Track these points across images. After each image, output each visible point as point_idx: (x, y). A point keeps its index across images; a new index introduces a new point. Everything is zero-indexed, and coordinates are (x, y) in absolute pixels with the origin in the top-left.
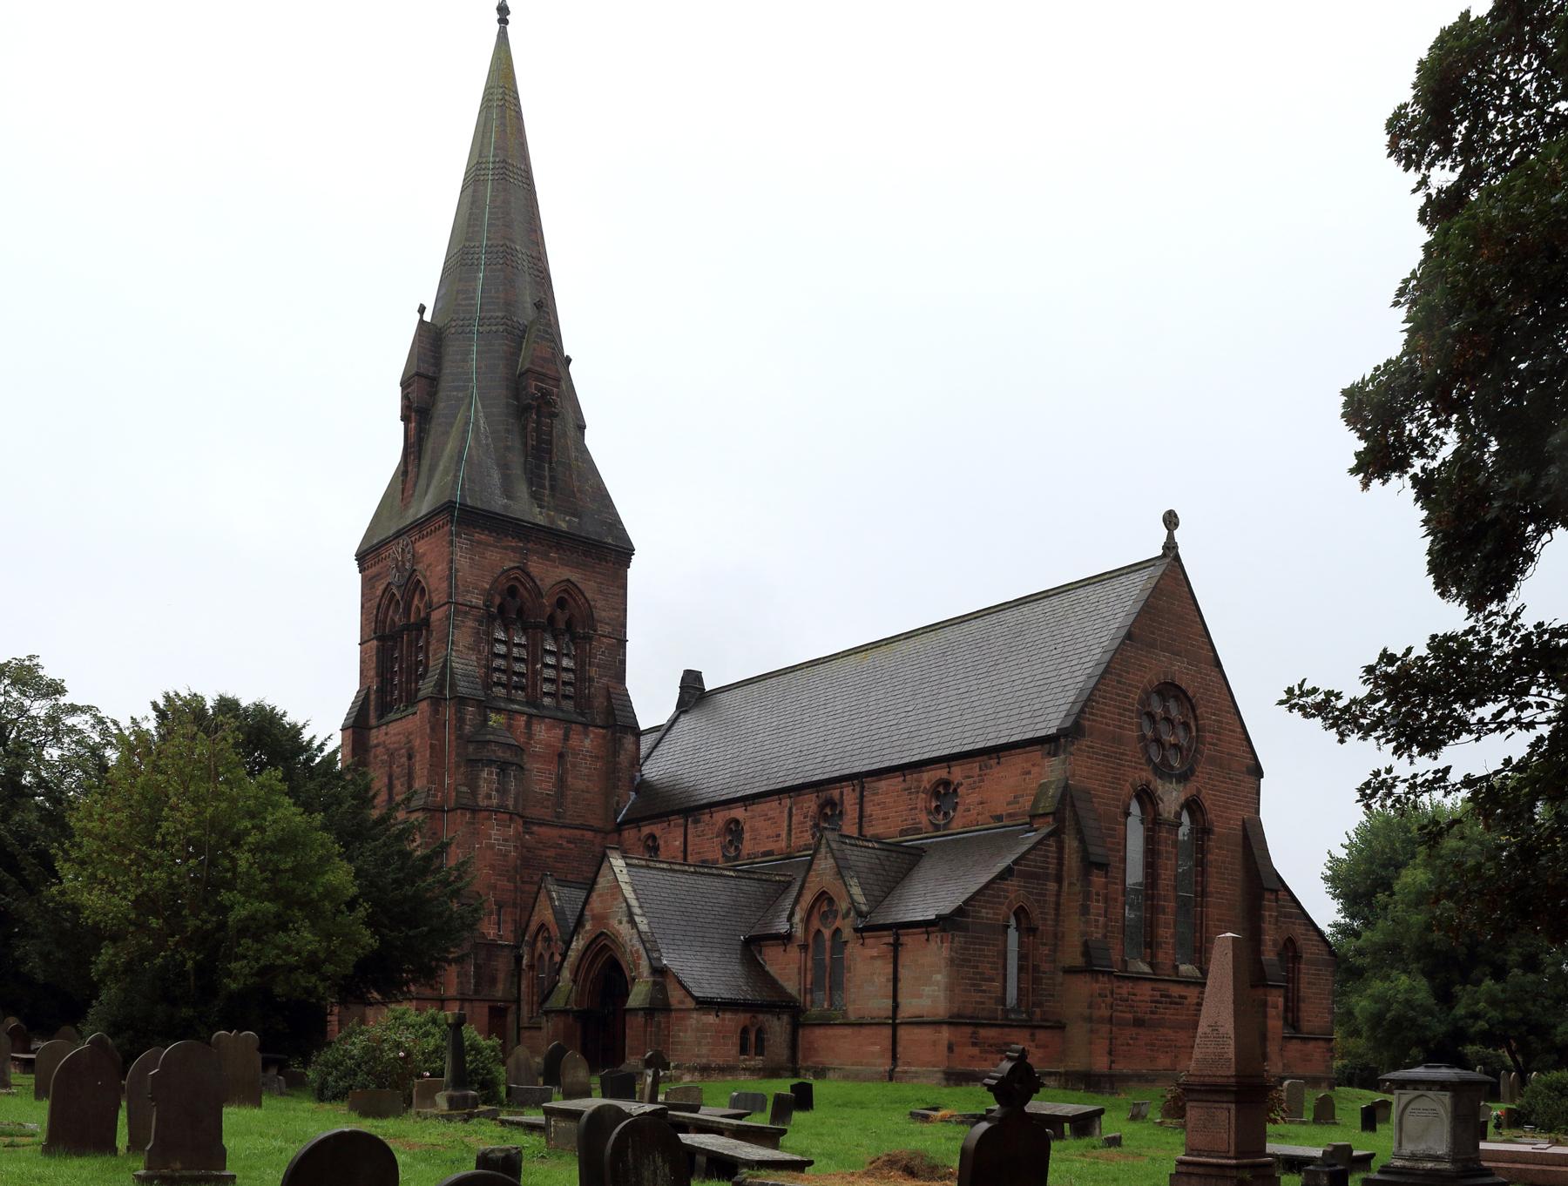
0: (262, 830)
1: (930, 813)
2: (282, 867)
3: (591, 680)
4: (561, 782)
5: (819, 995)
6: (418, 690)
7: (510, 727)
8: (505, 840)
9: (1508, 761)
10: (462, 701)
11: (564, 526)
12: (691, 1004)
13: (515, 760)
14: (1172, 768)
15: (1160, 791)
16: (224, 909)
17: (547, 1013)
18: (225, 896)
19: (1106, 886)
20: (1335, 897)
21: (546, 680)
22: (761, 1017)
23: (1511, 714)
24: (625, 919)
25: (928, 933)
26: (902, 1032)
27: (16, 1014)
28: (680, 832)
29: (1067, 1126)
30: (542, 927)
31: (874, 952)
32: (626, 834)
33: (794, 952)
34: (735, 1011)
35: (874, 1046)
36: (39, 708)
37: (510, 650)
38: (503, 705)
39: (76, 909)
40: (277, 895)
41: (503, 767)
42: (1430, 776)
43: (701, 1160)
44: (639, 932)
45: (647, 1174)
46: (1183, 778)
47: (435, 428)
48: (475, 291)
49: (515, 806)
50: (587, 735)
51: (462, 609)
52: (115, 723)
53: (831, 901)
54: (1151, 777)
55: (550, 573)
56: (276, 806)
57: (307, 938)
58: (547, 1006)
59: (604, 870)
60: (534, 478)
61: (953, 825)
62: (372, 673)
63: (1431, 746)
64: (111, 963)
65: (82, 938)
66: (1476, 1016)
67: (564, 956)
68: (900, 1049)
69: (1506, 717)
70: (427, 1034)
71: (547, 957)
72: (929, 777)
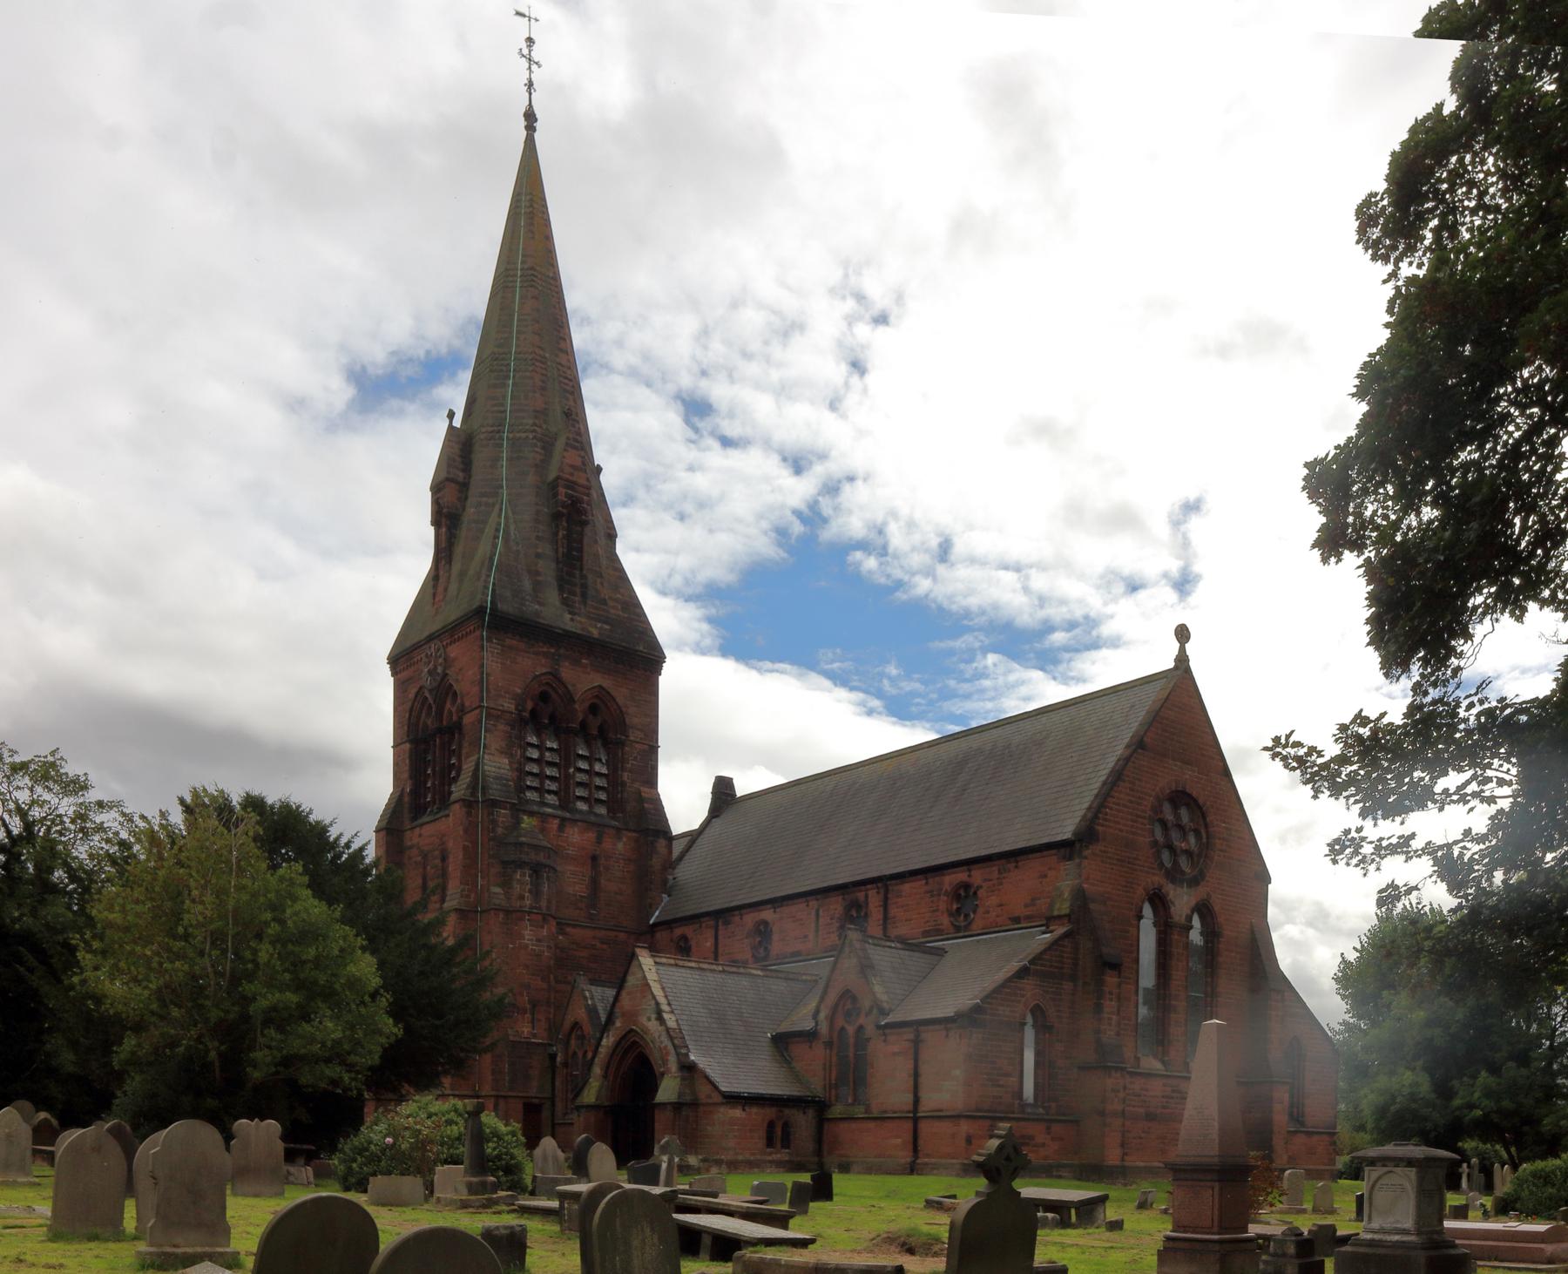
0: (282, 922)
1: (951, 914)
2: (304, 957)
3: (623, 784)
4: (595, 884)
6: (450, 793)
7: (543, 830)
8: (539, 940)
9: (1467, 832)
10: (494, 804)
11: (595, 633)
12: (717, 1098)
13: (548, 862)
14: (1183, 872)
15: (1171, 895)
16: (247, 1000)
17: (578, 1108)
18: (248, 988)
19: (1119, 985)
20: (1344, 997)
21: (580, 784)
22: (787, 1111)
23: (1473, 787)
24: (653, 1016)
25: (947, 1030)
26: (923, 1126)
27: (49, 1109)
28: (710, 934)
29: (1073, 1212)
32: (658, 935)
33: (819, 1051)
36: (66, 806)
37: (542, 755)
38: (535, 808)
39: (98, 999)
40: (299, 985)
41: (536, 870)
42: (1394, 841)
43: (707, 1241)
44: (668, 1030)
45: (636, 1243)
46: (1194, 882)
47: (463, 533)
48: (504, 397)
49: (548, 908)
50: (620, 839)
51: (494, 715)
52: (143, 817)
53: (854, 999)
54: (1163, 881)
55: (583, 680)
56: (295, 899)
57: (329, 1028)
58: (579, 1102)
59: (633, 968)
60: (564, 583)
61: (974, 926)
62: (406, 775)
63: (1396, 811)
64: (133, 1053)
65: (104, 1029)
66: (1471, 1106)
67: (595, 1052)
68: (921, 1142)
69: (1469, 790)
70: (450, 1122)
72: (950, 880)
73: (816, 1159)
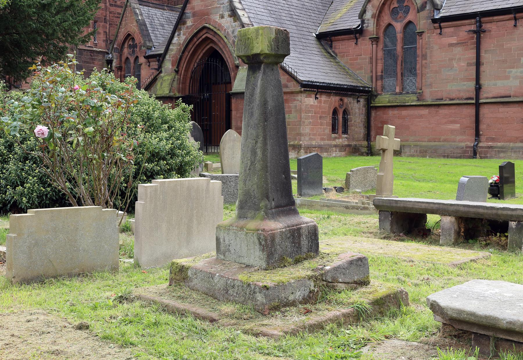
5: (389, 82)
12: (298, 88)
24: (227, 14)
25: (515, 19)
26: (485, 111)
30: (128, 36)
31: (453, 40)
33: (365, 45)
34: (329, 94)
35: (455, 126)
68: (482, 127)
71: (132, 60)
73: (365, 143)
